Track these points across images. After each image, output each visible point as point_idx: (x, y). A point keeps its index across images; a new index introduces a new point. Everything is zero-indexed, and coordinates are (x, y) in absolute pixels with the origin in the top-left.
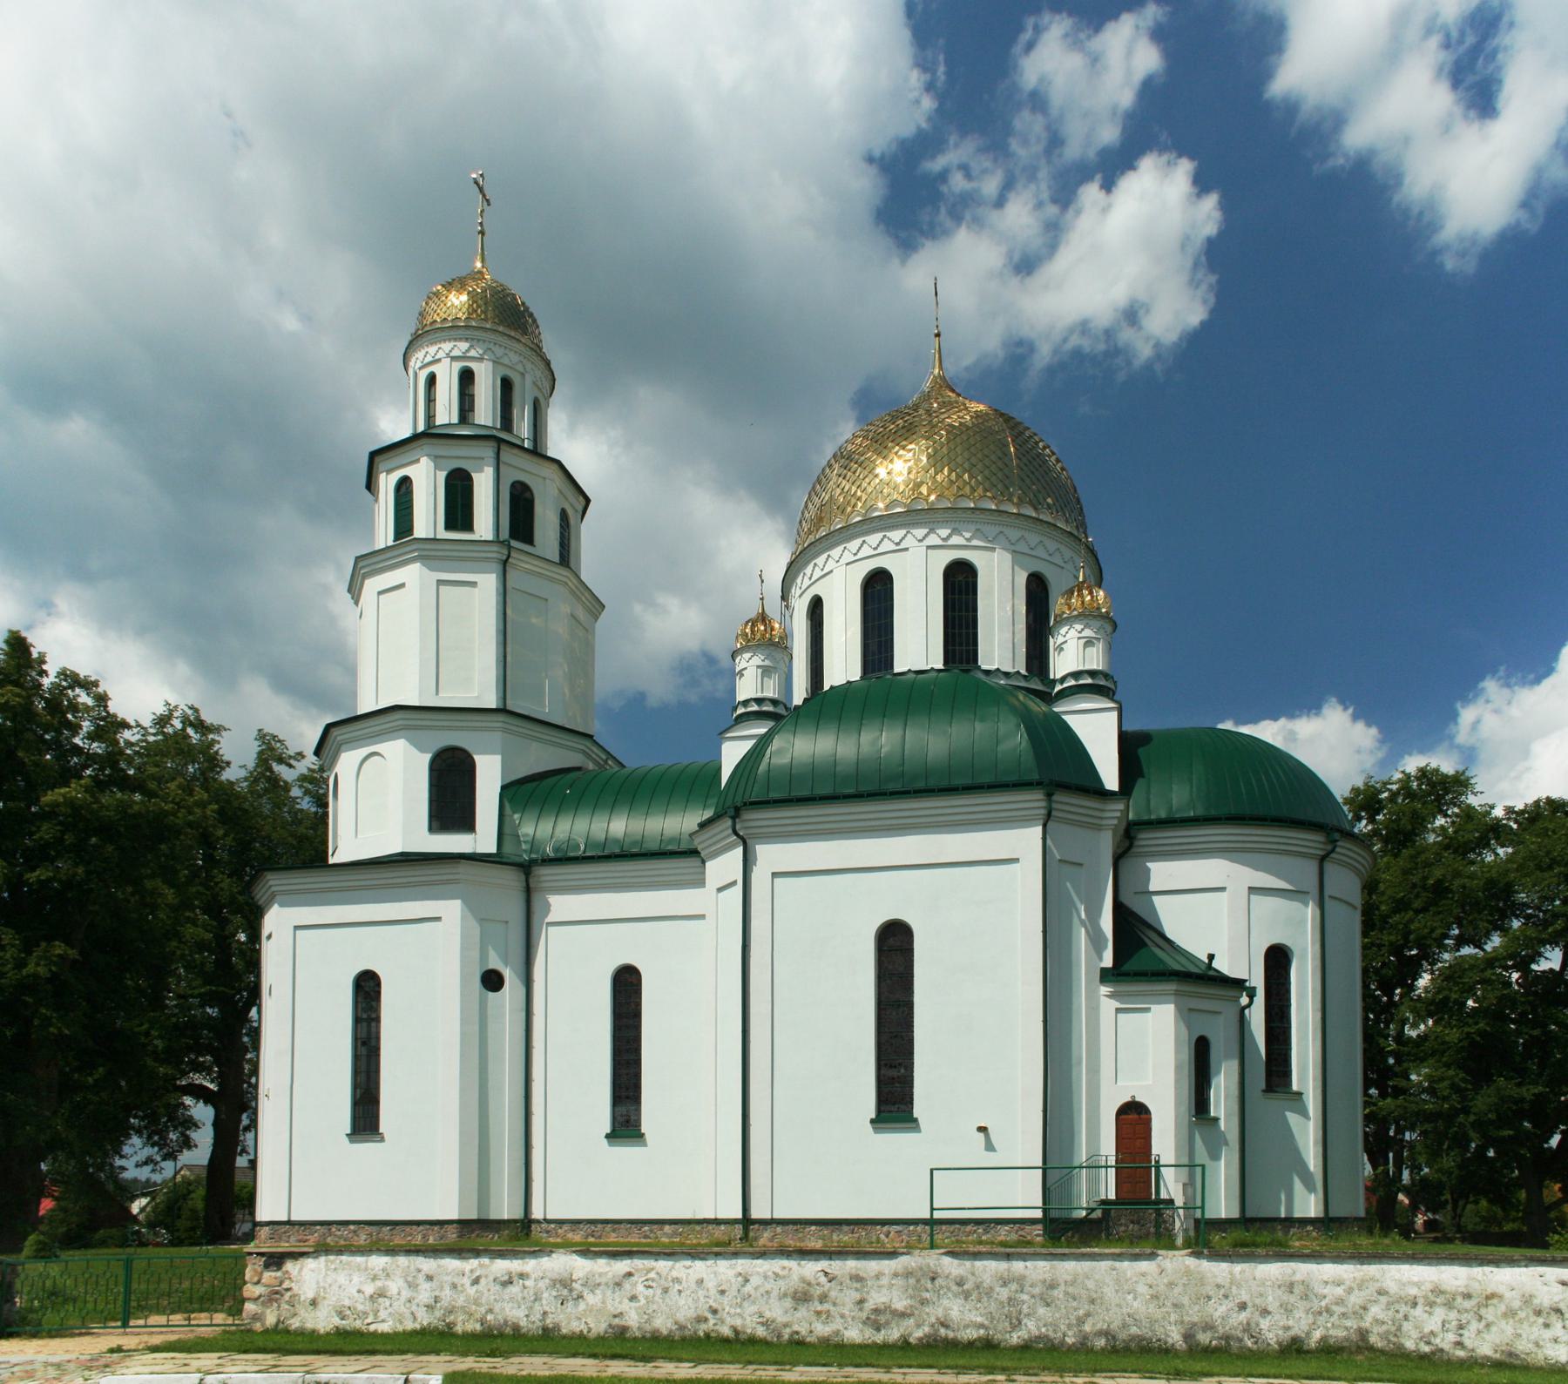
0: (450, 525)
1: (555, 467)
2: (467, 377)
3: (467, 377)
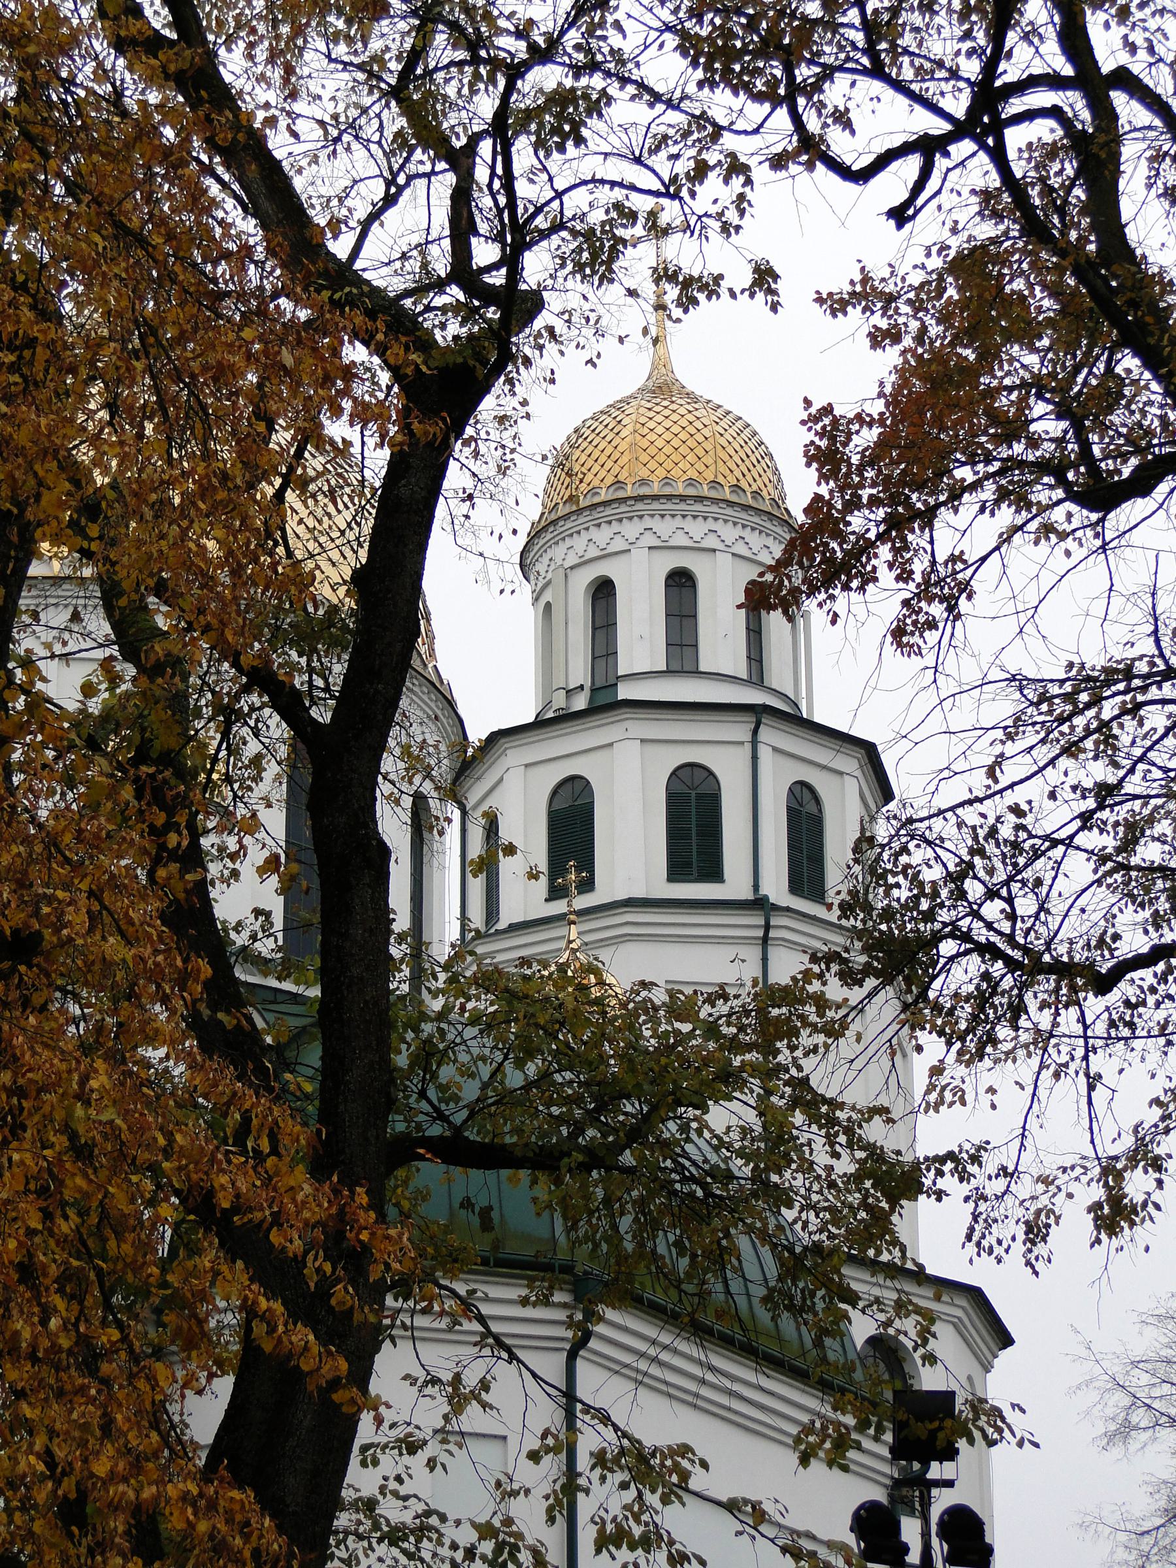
0: (678, 870)
1: (860, 753)
2: (681, 582)
3: (681, 582)
